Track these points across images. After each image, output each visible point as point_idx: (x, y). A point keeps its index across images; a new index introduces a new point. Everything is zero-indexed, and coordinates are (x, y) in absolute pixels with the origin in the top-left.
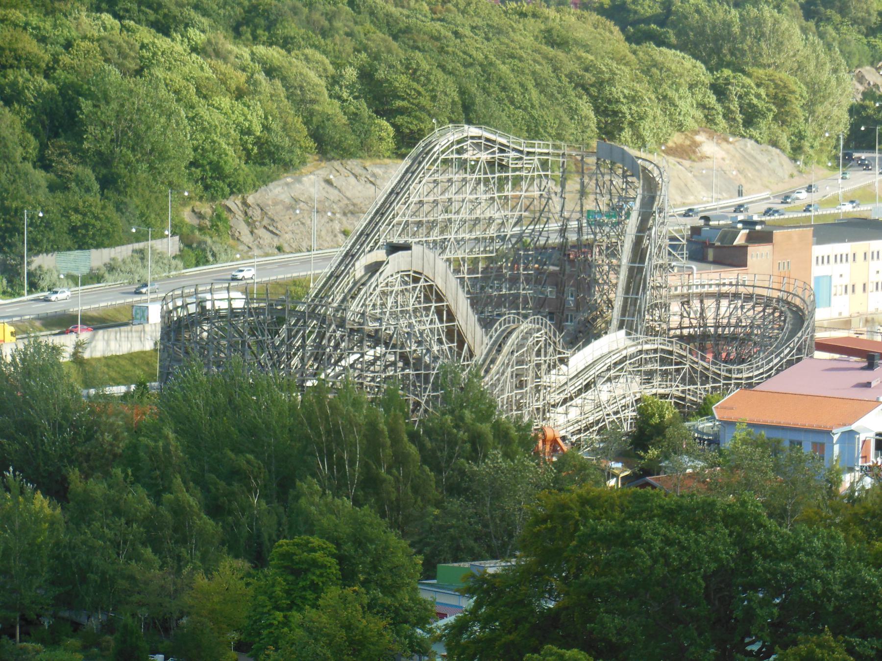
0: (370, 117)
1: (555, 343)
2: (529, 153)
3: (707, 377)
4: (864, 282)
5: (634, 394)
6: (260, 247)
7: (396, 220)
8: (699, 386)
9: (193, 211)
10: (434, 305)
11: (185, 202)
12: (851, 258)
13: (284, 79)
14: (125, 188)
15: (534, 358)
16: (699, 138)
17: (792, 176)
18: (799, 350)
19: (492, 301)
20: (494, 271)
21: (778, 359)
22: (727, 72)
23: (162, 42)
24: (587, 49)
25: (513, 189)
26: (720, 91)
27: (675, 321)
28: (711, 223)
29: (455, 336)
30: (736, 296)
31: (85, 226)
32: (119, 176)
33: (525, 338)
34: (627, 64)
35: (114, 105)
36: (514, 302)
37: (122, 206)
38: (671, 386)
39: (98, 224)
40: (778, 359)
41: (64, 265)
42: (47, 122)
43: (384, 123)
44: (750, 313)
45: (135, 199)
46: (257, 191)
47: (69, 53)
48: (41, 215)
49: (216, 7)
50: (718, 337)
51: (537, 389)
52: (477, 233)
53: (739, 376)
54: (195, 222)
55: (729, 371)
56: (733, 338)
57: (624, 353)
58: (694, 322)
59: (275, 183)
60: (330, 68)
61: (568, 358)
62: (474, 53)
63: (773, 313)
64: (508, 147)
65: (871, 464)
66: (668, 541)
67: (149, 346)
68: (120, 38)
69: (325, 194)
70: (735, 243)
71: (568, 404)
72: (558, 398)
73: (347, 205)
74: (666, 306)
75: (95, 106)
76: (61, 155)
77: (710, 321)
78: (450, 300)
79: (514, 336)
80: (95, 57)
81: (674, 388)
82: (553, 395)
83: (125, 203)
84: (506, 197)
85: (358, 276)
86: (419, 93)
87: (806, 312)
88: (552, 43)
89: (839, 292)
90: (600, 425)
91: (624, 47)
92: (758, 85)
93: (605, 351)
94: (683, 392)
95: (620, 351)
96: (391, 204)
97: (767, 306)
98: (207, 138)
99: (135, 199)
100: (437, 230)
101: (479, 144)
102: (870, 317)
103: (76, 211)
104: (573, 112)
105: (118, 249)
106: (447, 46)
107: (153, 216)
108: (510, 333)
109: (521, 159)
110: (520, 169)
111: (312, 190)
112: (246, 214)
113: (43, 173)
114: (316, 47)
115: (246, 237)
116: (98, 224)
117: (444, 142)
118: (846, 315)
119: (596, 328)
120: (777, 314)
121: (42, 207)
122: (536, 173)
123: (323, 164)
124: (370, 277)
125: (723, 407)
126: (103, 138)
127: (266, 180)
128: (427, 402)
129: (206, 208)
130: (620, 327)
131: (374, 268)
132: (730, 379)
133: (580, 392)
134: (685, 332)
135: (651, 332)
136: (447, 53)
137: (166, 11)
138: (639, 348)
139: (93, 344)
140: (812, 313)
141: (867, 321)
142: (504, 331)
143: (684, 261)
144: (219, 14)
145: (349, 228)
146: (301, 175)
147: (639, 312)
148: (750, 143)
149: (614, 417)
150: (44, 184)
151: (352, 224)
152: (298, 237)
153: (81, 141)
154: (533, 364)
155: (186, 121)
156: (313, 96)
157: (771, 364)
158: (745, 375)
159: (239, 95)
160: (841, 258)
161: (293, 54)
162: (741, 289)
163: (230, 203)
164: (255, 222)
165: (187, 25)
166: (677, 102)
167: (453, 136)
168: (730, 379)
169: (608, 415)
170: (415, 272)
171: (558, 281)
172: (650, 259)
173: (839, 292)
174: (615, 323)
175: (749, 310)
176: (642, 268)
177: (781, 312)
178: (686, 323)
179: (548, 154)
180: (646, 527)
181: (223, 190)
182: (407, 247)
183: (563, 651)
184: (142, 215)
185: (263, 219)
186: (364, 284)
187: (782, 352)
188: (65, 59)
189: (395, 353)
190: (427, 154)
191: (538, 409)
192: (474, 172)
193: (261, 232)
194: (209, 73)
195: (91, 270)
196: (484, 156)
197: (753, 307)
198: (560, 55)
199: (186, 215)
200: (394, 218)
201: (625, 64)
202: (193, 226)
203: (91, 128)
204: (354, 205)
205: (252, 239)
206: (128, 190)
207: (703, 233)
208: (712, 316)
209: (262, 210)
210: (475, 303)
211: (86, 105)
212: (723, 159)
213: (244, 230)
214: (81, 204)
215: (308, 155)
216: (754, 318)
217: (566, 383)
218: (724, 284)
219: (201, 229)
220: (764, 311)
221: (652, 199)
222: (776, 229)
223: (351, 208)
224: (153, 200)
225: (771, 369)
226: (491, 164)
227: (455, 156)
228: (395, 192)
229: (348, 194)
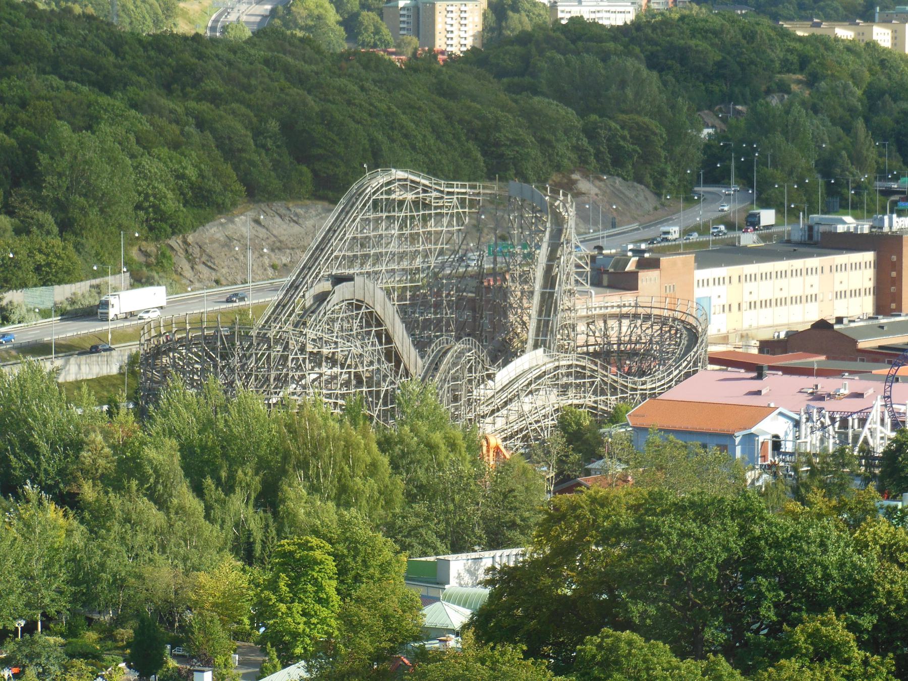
0: (291, 163)
1: (483, 361)
2: (449, 193)
3: (615, 389)
4: (740, 301)
5: (553, 404)
6: (200, 281)
7: (334, 254)
8: (609, 397)
9: (140, 250)
10: (374, 329)
11: (131, 242)
12: (727, 280)
13: (213, 131)
14: (81, 230)
15: (467, 374)
16: (575, 177)
17: (656, 209)
18: (695, 364)
19: (418, 325)
20: (421, 297)
21: (677, 371)
22: (594, 117)
23: (104, 100)
24: (474, 98)
25: (435, 226)
26: (591, 133)
27: (581, 340)
28: (604, 252)
29: (393, 356)
30: (636, 316)
31: (48, 265)
32: (75, 220)
33: (458, 357)
34: (509, 111)
35: (67, 157)
36: (438, 325)
37: (79, 247)
38: (585, 397)
39: (60, 263)
40: (677, 371)
41: (31, 300)
42: (9, 172)
43: (304, 169)
44: (647, 332)
45: (90, 240)
46: (195, 231)
47: (27, 111)
48: (11, 256)
49: (148, 68)
50: (620, 352)
51: (469, 402)
52: (405, 264)
53: (643, 387)
54: (142, 259)
55: (634, 383)
56: (634, 354)
57: (543, 369)
58: (599, 340)
59: (210, 224)
60: (255, 120)
61: (494, 374)
62: (377, 104)
63: (669, 331)
64: (431, 188)
65: (769, 462)
66: (683, 535)
67: (114, 370)
68: (68, 95)
69: (255, 233)
70: (626, 270)
71: (496, 414)
72: (486, 410)
73: (274, 242)
74: (574, 327)
75: (52, 158)
76: (23, 201)
77: (614, 340)
78: (389, 326)
79: (449, 355)
80: (49, 114)
81: (587, 399)
82: (482, 407)
83: (82, 244)
84: (429, 232)
85: (307, 305)
86: (334, 141)
87: (700, 330)
88: (443, 95)
89: (717, 312)
90: (524, 433)
91: (504, 97)
92: (623, 128)
93: (526, 367)
94: (595, 402)
95: (538, 367)
96: (329, 240)
97: (664, 324)
98: (149, 184)
99: (90, 240)
100: (370, 261)
101: (405, 185)
102: (744, 333)
103: (40, 251)
104: (466, 154)
105: (78, 285)
106: (354, 99)
107: (107, 255)
108: (446, 353)
109: (442, 198)
110: (441, 207)
111: (244, 229)
112: (187, 251)
113: (8, 219)
114: (242, 102)
115: (188, 273)
116: (60, 263)
117: (375, 184)
118: (724, 331)
119: (513, 347)
120: (673, 332)
121: (12, 249)
122: (455, 211)
123: (251, 206)
124: (319, 306)
125: (634, 415)
126: (60, 186)
127: (203, 221)
128: (378, 416)
129: (151, 248)
130: (536, 346)
131: (322, 298)
132: (636, 390)
133: (506, 404)
134: (591, 349)
135: (561, 348)
136: (354, 104)
137: (105, 72)
138: (557, 364)
139: (67, 368)
140: (705, 331)
141: (742, 336)
142: (439, 351)
143: (588, 286)
144: (150, 74)
145: (277, 262)
146: (234, 216)
147: (552, 332)
148: (618, 181)
149: (536, 426)
150: (10, 228)
151: (280, 259)
152: (233, 271)
153: (39, 188)
154: (466, 380)
155: (131, 169)
156: (240, 146)
157: (671, 377)
158: (649, 386)
159: (175, 146)
160: (719, 281)
161: (221, 108)
162: (640, 310)
163: (172, 242)
164: (195, 258)
165: (125, 85)
166: (555, 144)
167: (382, 179)
168: (636, 390)
169: (530, 424)
170: (357, 300)
171: (473, 306)
172: (560, 285)
173: (717, 312)
174: (531, 342)
175: (648, 328)
176: (553, 293)
177: (677, 330)
178: (592, 340)
179: (465, 193)
180: (664, 522)
181: (165, 231)
182: (350, 278)
183: (619, 633)
184: (97, 254)
185: (201, 256)
186: (313, 312)
187: (681, 365)
188: (23, 116)
189: (350, 373)
190: (360, 195)
191: (470, 420)
192: (401, 211)
193: (200, 267)
194: (147, 127)
195: (55, 304)
196: (410, 196)
197: (652, 326)
198: (452, 104)
199: (134, 253)
200: (332, 253)
201: (507, 112)
202: (141, 264)
203: (49, 178)
204: (280, 242)
205: (193, 274)
206: (83, 232)
207: (597, 261)
208: (615, 335)
209: (200, 247)
210: (410, 326)
211: (44, 158)
212: (597, 195)
213: (186, 266)
214: (44, 244)
215: (238, 198)
216: (652, 335)
217: (493, 396)
218: (624, 306)
219: (148, 265)
220: (661, 329)
221: (560, 232)
222: (665, 255)
223: (278, 244)
224: (106, 240)
225: (672, 380)
226: (416, 203)
227: (384, 197)
228: (332, 230)
229: (275, 232)
